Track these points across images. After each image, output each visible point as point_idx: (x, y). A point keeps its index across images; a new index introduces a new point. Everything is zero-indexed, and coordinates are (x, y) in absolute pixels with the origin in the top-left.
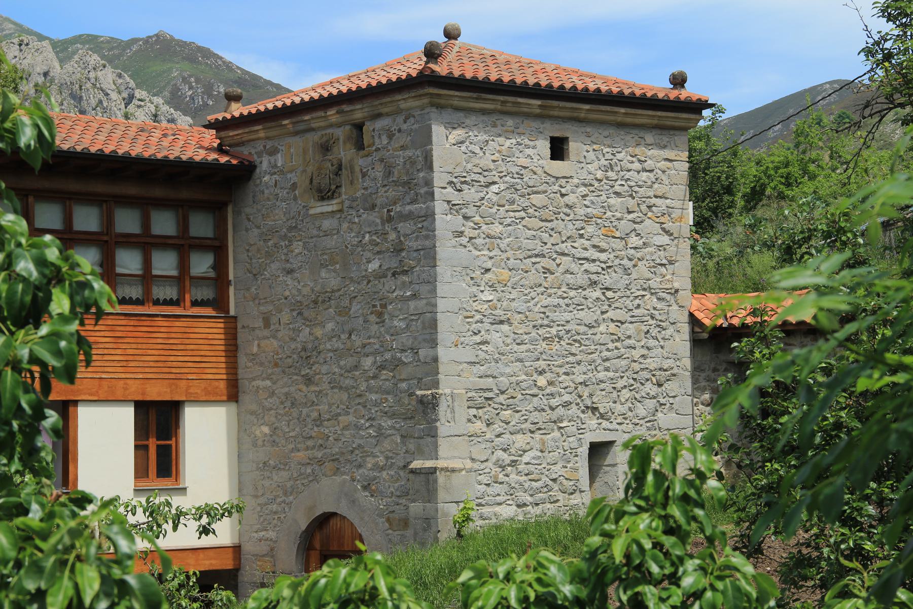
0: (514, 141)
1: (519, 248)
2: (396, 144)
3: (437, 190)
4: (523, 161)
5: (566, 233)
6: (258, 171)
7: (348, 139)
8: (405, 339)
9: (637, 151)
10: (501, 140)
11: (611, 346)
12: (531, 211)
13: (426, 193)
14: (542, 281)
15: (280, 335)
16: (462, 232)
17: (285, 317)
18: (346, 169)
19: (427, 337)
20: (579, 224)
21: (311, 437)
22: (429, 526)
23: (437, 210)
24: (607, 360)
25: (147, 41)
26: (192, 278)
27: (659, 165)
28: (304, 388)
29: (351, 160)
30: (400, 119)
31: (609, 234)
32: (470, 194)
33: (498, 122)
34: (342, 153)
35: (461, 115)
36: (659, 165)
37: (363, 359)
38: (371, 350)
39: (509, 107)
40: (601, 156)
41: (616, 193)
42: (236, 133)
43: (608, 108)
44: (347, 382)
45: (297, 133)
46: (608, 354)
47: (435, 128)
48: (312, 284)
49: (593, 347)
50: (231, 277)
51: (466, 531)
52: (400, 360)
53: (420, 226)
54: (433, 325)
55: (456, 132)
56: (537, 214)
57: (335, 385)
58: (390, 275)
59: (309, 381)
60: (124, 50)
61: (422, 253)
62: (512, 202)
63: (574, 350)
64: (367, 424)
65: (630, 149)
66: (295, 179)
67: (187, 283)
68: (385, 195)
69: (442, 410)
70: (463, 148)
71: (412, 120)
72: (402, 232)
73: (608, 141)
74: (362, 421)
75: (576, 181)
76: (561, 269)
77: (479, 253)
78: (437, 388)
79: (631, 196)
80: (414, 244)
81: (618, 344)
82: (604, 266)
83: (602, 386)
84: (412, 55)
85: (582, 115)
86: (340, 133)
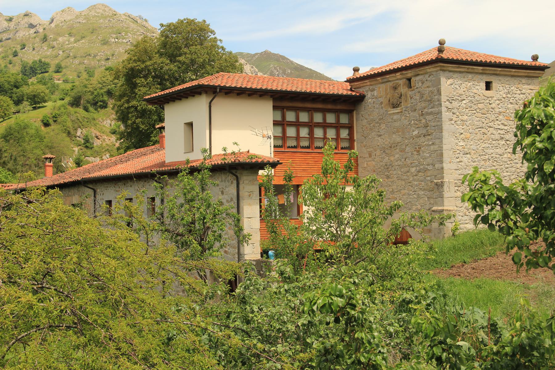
0: (471, 83)
1: (474, 125)
2: (425, 85)
3: (443, 103)
4: (475, 91)
5: (491, 119)
6: (366, 98)
7: (404, 84)
8: (429, 160)
9: (519, 86)
10: (467, 83)
11: (509, 163)
12: (478, 110)
13: (438, 104)
14: (482, 137)
15: (376, 160)
16: (452, 119)
17: (378, 152)
18: (404, 96)
19: (439, 159)
20: (496, 115)
21: (389, 198)
22: (441, 232)
23: (443, 111)
24: (507, 168)
25: (261, 53)
26: (341, 139)
27: (527, 91)
28: (386, 180)
29: (406, 92)
30: (427, 76)
31: (508, 119)
32: (455, 104)
33: (466, 76)
34: (402, 90)
35: (452, 73)
36: (527, 91)
37: (411, 169)
38: (414, 165)
39: (470, 71)
40: (505, 89)
41: (510, 103)
42: (358, 83)
43: (508, 70)
44: (404, 177)
45: (383, 83)
46: (508, 166)
47: (441, 79)
48: (389, 140)
49: (502, 163)
50: (355, 138)
51: (456, 233)
52: (427, 168)
53: (435, 117)
54: (442, 155)
55: (449, 80)
56: (480, 111)
57: (399, 178)
58: (422, 136)
59: (388, 177)
60: (253, 57)
61: (436, 127)
62: (471, 107)
63: (494, 164)
64: (413, 193)
65: (516, 86)
66: (382, 100)
67: (339, 140)
68: (420, 106)
69: (445, 187)
70: (452, 87)
71: (432, 76)
72: (428, 119)
73: (508, 83)
74: (411, 192)
75: (495, 98)
76: (490, 133)
77: (458, 127)
78: (443, 179)
79: (516, 104)
80: (433, 124)
81: (511, 162)
82: (506, 131)
83: (505, 178)
84: (426, 51)
85: (498, 73)
86: (401, 82)
